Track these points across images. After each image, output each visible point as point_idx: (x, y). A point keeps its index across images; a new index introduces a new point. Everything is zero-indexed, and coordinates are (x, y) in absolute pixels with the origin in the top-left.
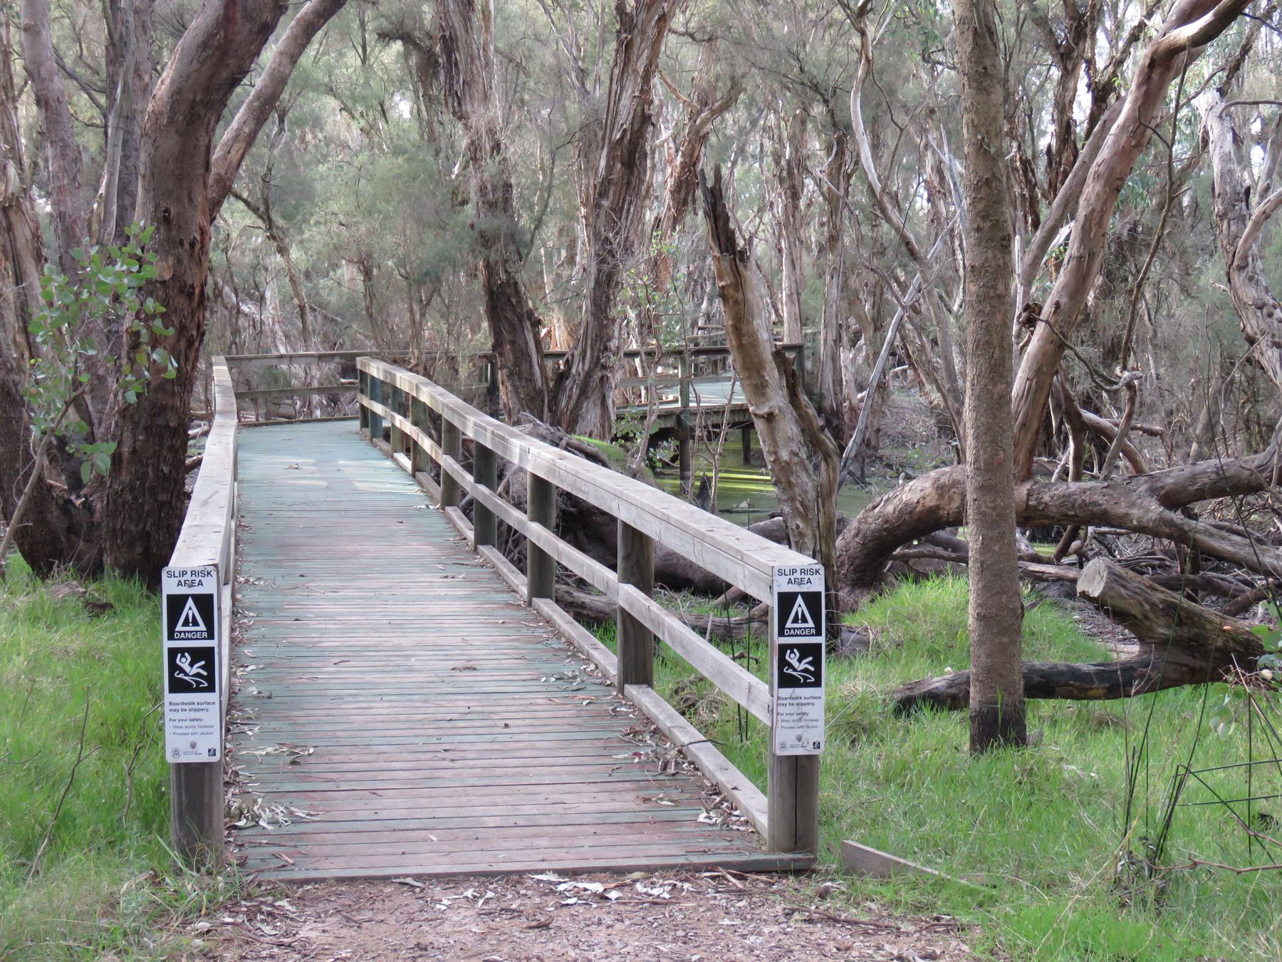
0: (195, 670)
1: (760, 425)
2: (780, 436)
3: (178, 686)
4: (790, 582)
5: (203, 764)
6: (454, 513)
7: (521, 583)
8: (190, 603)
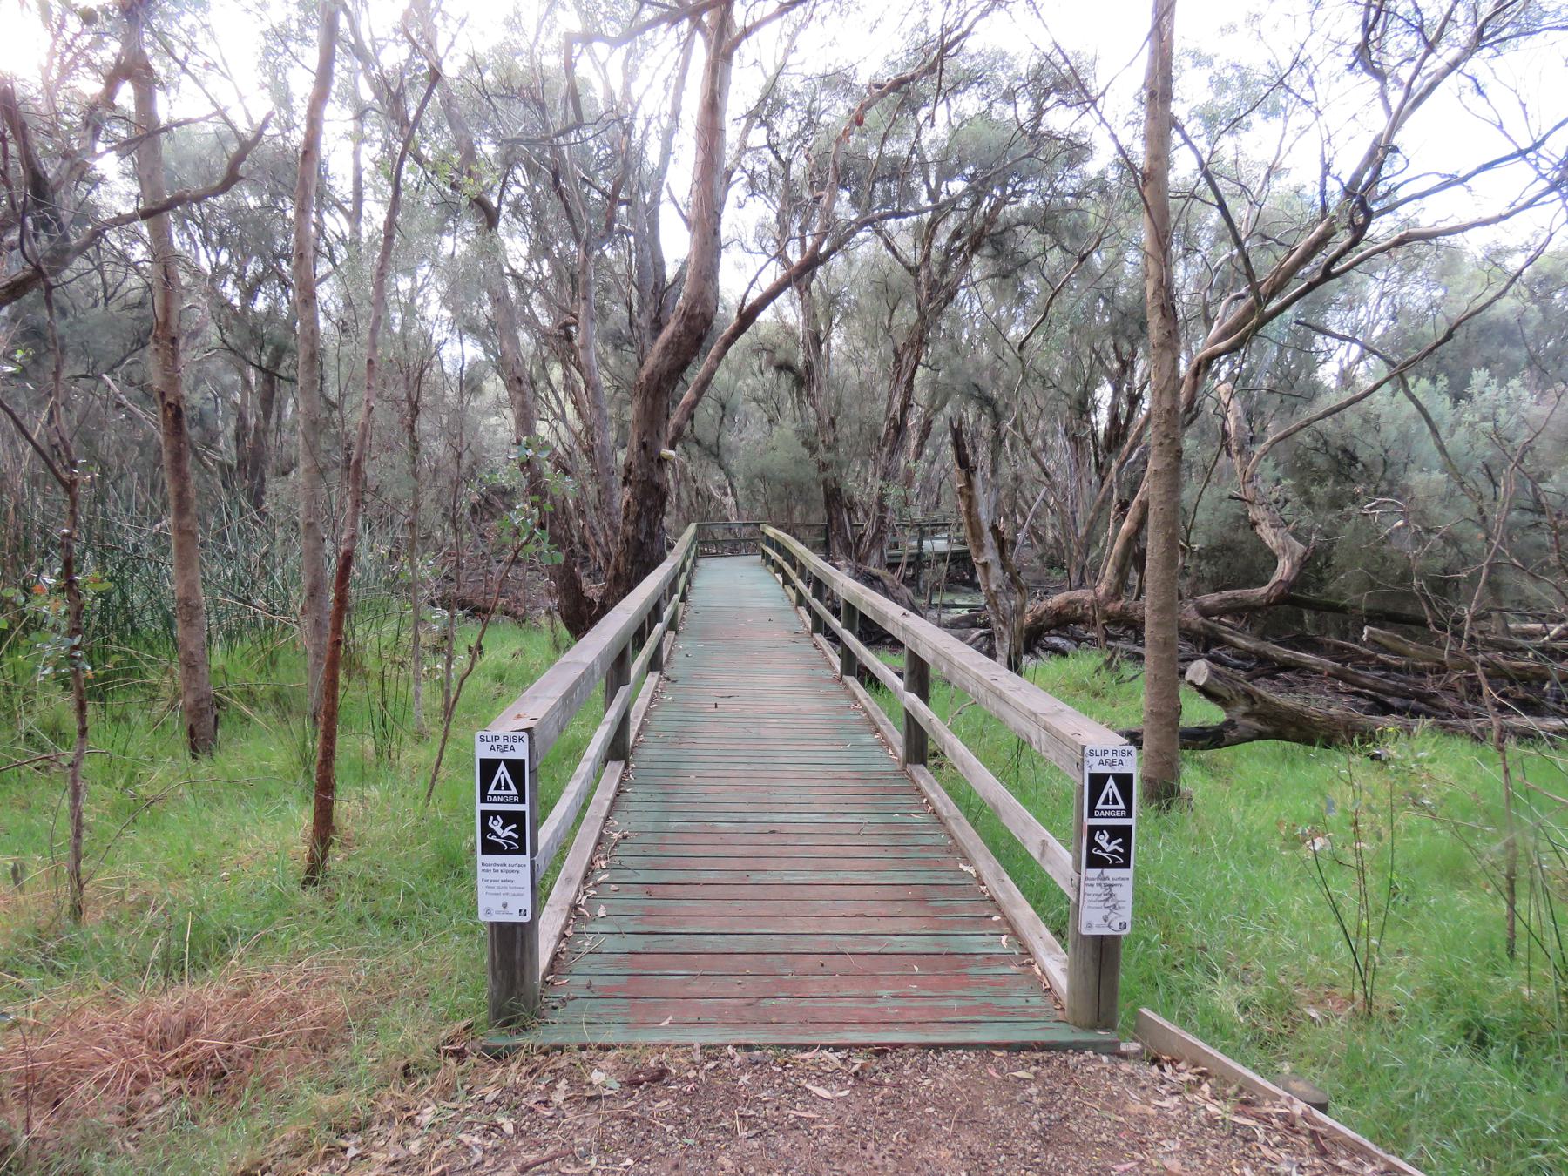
0: (507, 833)
1: (979, 569)
2: (991, 575)
3: (490, 847)
4: (1101, 763)
5: (515, 924)
6: (802, 610)
7: (837, 662)
8: (502, 767)
